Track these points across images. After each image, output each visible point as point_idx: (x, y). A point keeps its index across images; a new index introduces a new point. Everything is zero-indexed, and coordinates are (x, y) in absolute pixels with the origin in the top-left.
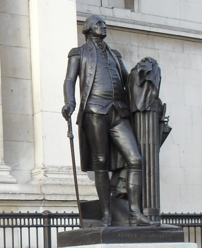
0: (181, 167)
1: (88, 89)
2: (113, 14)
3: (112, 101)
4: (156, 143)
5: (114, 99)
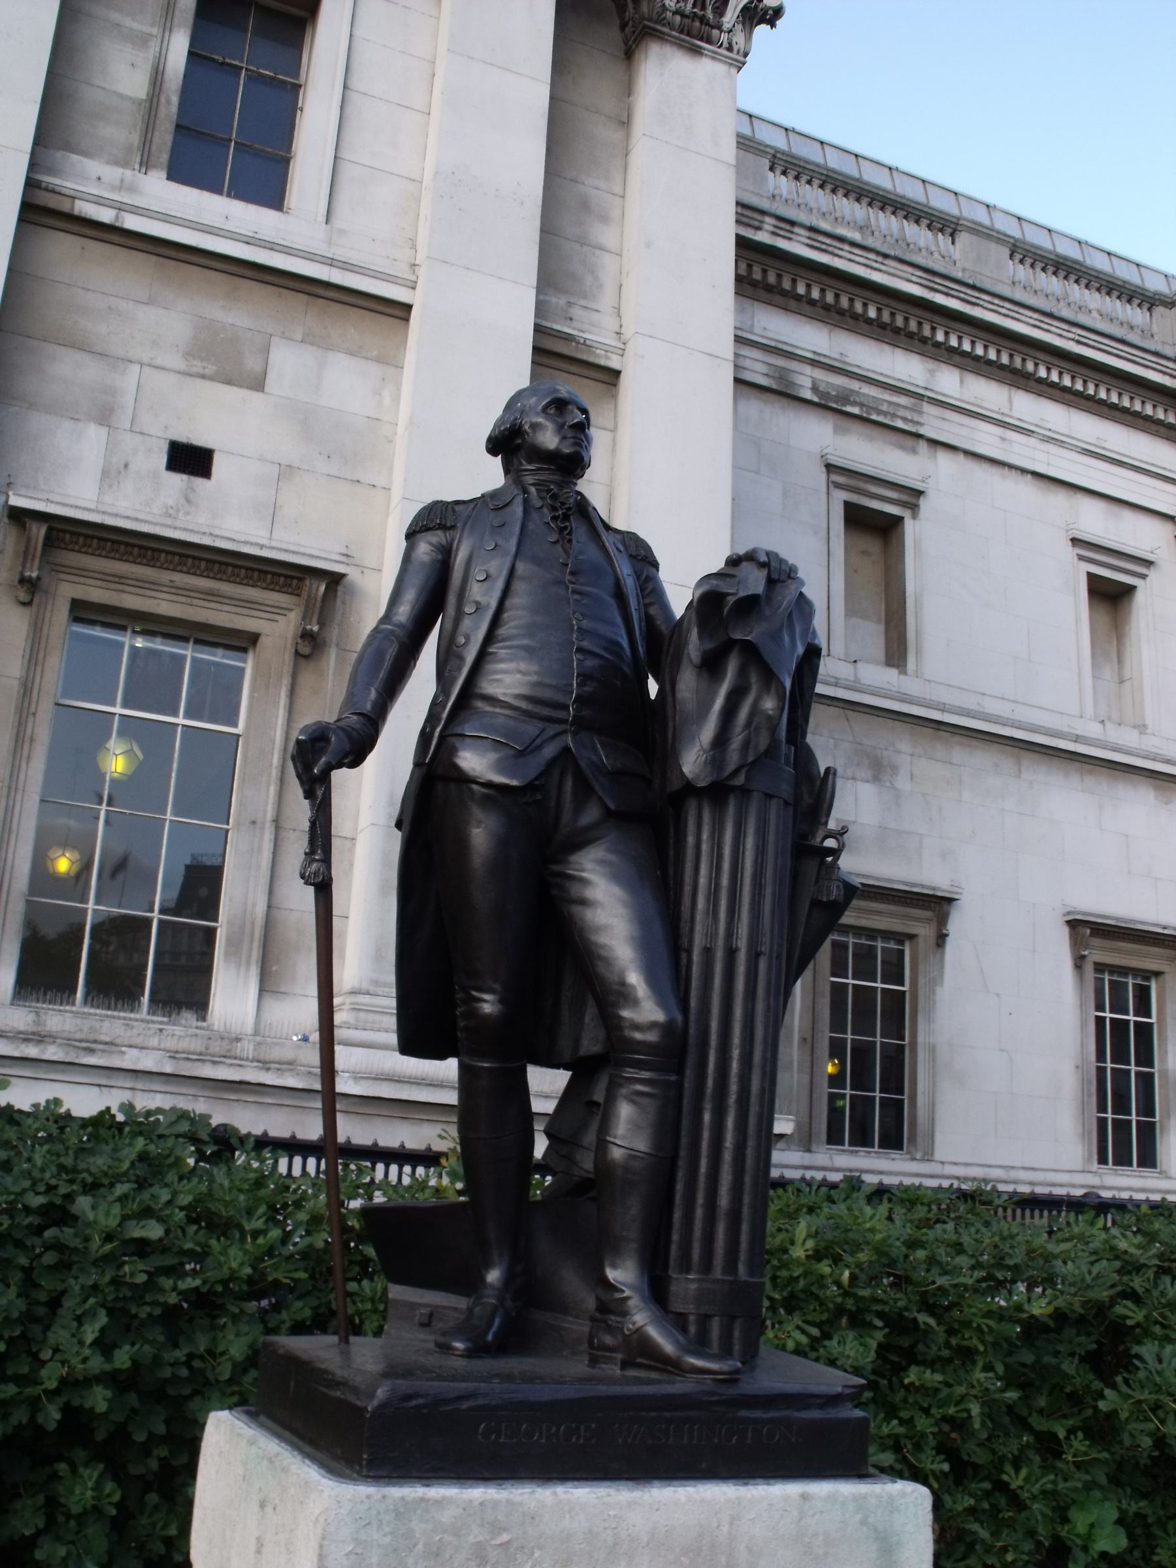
0: (1001, 1050)
1: (460, 669)
2: (856, 675)
3: (564, 732)
4: (765, 948)
5: (573, 723)
